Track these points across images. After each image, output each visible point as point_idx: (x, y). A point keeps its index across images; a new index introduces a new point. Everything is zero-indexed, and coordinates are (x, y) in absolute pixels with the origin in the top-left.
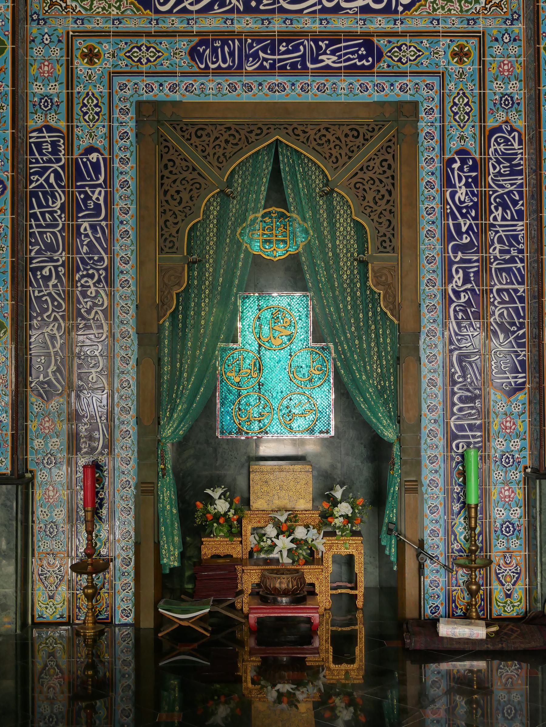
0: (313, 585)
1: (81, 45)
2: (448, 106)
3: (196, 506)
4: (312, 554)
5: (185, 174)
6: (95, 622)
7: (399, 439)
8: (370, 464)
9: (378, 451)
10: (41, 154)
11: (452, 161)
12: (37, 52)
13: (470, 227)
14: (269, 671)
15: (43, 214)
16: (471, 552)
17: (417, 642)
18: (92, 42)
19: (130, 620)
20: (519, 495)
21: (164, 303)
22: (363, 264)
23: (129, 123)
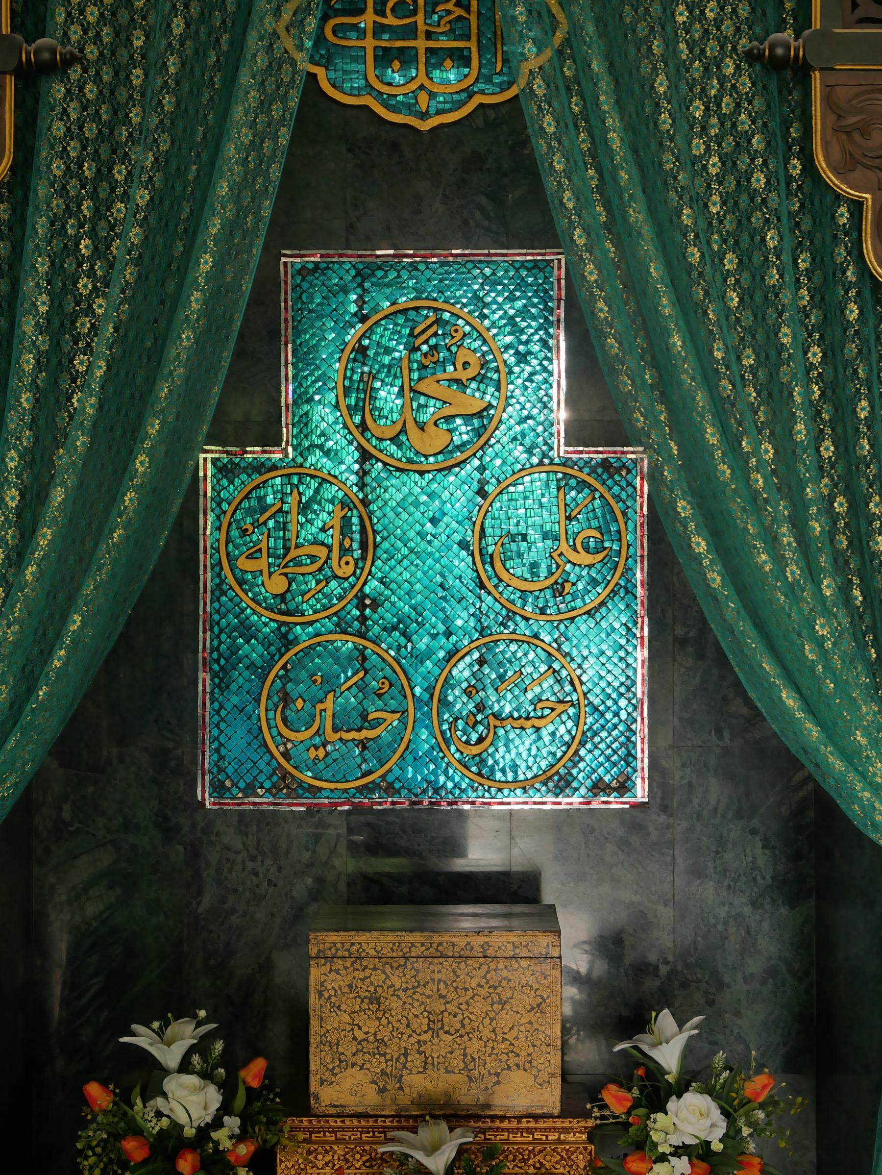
3: (84, 1100)
8: (784, 911)
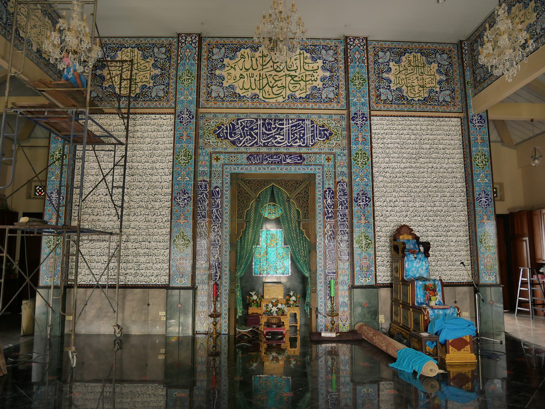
1: (214, 156)
2: (325, 175)
6: (216, 333)
9: (304, 280)
11: (326, 191)
12: (201, 158)
13: (332, 211)
14: (269, 349)
17: (315, 338)
18: (217, 155)
19: (227, 333)
20: (347, 294)
22: (299, 222)
23: (228, 180)
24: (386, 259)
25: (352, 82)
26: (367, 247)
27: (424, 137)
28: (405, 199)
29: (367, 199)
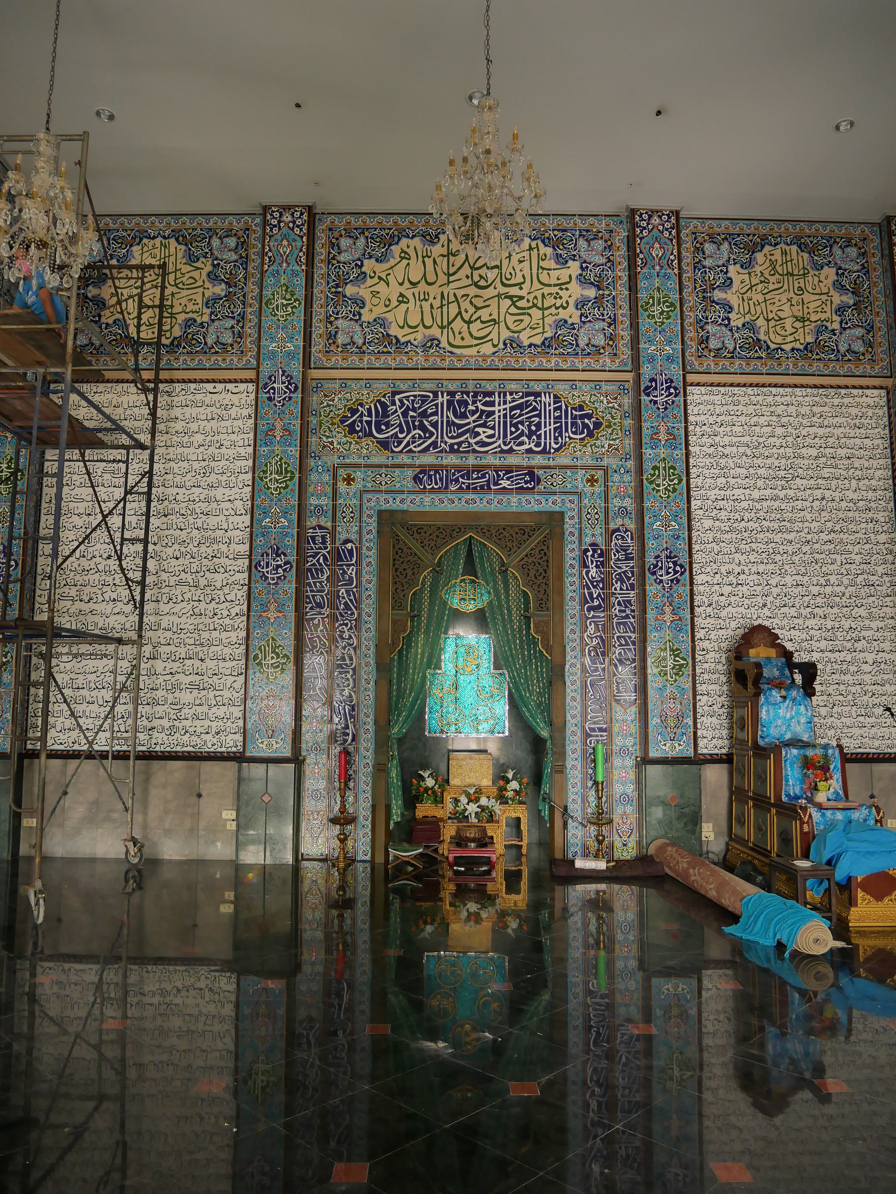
0: (492, 838)
1: (343, 473)
4: (491, 816)
5: (410, 558)
6: (345, 858)
7: (551, 737)
9: (537, 746)
10: (314, 543)
11: (587, 550)
12: (313, 477)
13: (599, 595)
14: (462, 893)
15: (315, 583)
16: (599, 814)
17: (562, 871)
18: (350, 471)
20: (632, 776)
21: (395, 643)
23: (372, 524)
24: (719, 699)
25: (646, 310)
26: (676, 674)
27: (804, 432)
28: (761, 568)
29: (678, 568)
